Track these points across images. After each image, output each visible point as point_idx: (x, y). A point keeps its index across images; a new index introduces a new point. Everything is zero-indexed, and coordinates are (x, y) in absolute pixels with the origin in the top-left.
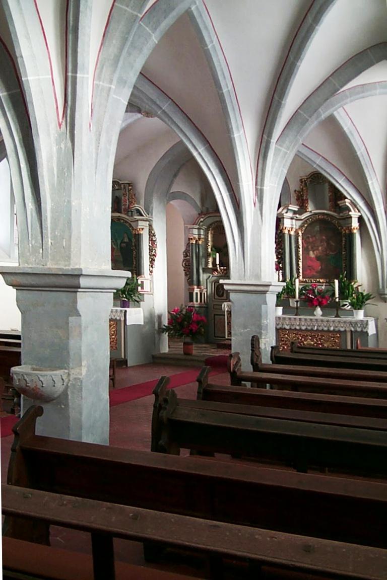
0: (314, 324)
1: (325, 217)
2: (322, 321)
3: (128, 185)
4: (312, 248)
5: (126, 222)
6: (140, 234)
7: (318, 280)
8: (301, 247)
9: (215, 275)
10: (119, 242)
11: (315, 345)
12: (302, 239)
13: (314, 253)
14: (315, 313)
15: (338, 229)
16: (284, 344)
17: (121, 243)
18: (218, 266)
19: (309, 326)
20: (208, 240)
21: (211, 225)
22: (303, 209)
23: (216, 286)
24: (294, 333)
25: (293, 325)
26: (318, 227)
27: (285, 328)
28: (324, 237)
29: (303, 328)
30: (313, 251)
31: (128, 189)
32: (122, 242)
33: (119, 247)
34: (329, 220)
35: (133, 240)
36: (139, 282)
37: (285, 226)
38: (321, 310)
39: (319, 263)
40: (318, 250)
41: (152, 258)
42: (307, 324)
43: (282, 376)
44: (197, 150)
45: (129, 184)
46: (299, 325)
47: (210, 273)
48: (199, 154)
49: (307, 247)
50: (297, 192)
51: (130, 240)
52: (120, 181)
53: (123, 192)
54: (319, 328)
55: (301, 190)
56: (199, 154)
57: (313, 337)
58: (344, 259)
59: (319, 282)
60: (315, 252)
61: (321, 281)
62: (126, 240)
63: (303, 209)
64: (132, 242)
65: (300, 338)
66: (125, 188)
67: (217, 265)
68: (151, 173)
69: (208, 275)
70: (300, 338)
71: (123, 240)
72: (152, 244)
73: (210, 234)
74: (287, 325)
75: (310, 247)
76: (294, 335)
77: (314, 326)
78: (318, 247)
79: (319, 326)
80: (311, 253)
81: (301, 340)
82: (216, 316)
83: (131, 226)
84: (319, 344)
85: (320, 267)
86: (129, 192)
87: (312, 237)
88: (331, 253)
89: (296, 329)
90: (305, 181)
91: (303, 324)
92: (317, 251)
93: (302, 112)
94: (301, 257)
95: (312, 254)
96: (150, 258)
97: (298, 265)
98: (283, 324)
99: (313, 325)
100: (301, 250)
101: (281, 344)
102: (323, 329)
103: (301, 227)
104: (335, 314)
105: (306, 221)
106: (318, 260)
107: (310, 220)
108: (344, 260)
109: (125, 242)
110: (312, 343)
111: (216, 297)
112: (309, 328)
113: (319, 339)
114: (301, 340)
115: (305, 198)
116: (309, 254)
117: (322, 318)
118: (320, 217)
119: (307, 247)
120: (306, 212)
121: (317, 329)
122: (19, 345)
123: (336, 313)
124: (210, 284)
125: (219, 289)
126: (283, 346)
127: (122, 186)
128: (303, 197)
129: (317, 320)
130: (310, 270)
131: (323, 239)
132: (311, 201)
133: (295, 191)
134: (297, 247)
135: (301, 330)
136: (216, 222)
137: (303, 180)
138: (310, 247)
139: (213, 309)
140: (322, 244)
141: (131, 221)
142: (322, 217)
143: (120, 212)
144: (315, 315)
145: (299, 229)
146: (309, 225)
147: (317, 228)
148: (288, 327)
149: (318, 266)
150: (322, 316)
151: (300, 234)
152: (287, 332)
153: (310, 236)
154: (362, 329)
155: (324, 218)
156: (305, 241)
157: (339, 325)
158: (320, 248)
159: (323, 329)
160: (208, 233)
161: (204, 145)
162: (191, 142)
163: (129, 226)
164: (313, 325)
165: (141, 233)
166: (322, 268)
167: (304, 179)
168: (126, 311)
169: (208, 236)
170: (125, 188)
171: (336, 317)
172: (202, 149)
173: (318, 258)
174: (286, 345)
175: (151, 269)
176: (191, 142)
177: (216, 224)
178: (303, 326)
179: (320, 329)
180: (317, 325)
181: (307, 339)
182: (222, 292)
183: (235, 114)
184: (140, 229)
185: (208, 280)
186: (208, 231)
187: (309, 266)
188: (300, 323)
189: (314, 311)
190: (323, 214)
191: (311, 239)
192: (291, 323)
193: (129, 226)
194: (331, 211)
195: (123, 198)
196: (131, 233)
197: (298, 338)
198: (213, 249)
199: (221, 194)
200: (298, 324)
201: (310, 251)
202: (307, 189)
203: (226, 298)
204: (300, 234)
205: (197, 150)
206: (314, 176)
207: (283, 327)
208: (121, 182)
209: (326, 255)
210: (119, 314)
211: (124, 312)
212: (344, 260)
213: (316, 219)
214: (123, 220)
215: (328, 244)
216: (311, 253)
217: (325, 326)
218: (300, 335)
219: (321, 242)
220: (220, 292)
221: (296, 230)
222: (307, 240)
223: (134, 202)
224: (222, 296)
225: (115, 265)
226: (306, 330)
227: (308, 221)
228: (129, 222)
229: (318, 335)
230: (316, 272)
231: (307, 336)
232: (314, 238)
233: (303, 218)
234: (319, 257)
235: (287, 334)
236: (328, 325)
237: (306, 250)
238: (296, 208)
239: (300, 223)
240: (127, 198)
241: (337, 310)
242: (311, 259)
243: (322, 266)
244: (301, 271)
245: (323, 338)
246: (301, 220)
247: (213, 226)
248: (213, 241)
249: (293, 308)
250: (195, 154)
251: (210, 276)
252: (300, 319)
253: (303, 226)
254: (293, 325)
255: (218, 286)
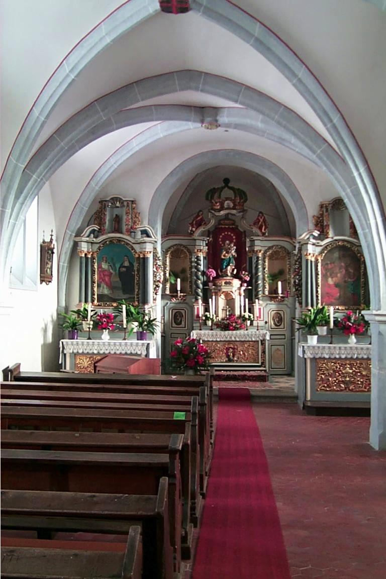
0: (354, 352)
1: (345, 243)
2: (357, 348)
3: (131, 202)
4: (331, 275)
5: (128, 244)
6: (147, 258)
7: (337, 307)
8: (320, 273)
9: (173, 302)
10: (118, 266)
11: (354, 373)
12: (322, 266)
13: (332, 280)
14: (349, 341)
15: (357, 256)
16: (322, 374)
17: (119, 268)
18: (179, 292)
19: (349, 354)
20: (166, 264)
21: (170, 248)
22: (323, 235)
23: (173, 314)
24: (332, 363)
25: (332, 354)
26: (337, 253)
27: (324, 357)
28: (343, 264)
29: (343, 357)
30: (332, 278)
31: (132, 206)
32: (122, 266)
33: (117, 271)
34: (349, 246)
35: (136, 265)
36: (147, 312)
37: (309, 252)
38: (355, 337)
39: (337, 290)
40: (337, 277)
41: (157, 284)
42: (358, 352)
43: (76, 403)
44: (358, 169)
45: (132, 201)
46: (339, 354)
47: (169, 300)
48: (360, 175)
49: (326, 273)
50: (315, 217)
51: (131, 264)
52: (124, 198)
53: (125, 209)
54: (358, 356)
55: (320, 216)
56: (360, 175)
57: (352, 366)
58: (363, 285)
59: (338, 309)
60: (334, 279)
61: (340, 308)
62: (126, 264)
63: (323, 235)
64: (133, 266)
65: (339, 367)
66: (128, 206)
67: (178, 291)
68: (157, 190)
69: (167, 301)
70: (339, 367)
71: (123, 263)
72: (156, 269)
73: (168, 258)
74: (327, 354)
75: (328, 274)
76: (333, 364)
77: (354, 355)
78: (337, 273)
79: (358, 354)
80: (330, 279)
81: (339, 368)
82: (273, 347)
83: (133, 249)
84: (358, 372)
85: (338, 294)
86: (132, 210)
87: (330, 263)
88: (349, 280)
89: (335, 358)
90: (326, 206)
91: (343, 352)
92: (336, 279)
93: (56, 136)
94: (320, 284)
95: (331, 281)
96: (154, 284)
97: (317, 292)
98: (322, 354)
99: (353, 353)
100: (320, 276)
101: (318, 374)
102: (363, 357)
103: (321, 253)
104: (88, 336)
105: (326, 247)
106: (336, 287)
107: (330, 246)
108: (363, 287)
109: (125, 267)
110: (351, 371)
111: (174, 325)
112: (349, 356)
113: (358, 367)
114: (339, 368)
115: (325, 224)
116: (327, 281)
117: (356, 346)
118: (340, 243)
119: (326, 273)
120: (327, 238)
121: (357, 357)
122: (3, 397)
123: (330, 340)
124: (168, 311)
125: (177, 316)
126: (321, 375)
127: (125, 203)
128: (323, 222)
129: (351, 348)
130: (328, 297)
131: (342, 266)
132: (332, 227)
133: (314, 217)
134: (317, 274)
135: (340, 358)
136: (175, 245)
137: (324, 205)
138: (328, 274)
139: (286, 340)
140: (341, 270)
141: (133, 243)
142: (342, 244)
143: (121, 233)
144: (349, 344)
145: (319, 255)
146: (329, 251)
147: (336, 255)
148: (327, 357)
149: (337, 293)
150: (356, 343)
151: (320, 261)
152: (326, 361)
153: (329, 262)
154: (368, 355)
155: (343, 245)
156: (324, 267)
157: (362, 353)
158: (339, 275)
159: (363, 357)
160: (166, 257)
161: (364, 165)
162: (354, 161)
163: (130, 249)
164: (353, 353)
165: (148, 256)
166: (340, 295)
167: (326, 204)
168: (148, 344)
169: (166, 261)
170: (128, 206)
171: (88, 339)
172: (362, 170)
173: (336, 285)
174: (323, 374)
175: (155, 296)
176: (354, 161)
177: (175, 247)
178: (343, 354)
179: (360, 357)
180: (356, 352)
181: (346, 368)
182: (180, 320)
183: (30, 133)
184: (257, 251)
185: (165, 307)
186: (167, 254)
187: (327, 293)
188: (339, 352)
189: (348, 339)
190: (344, 241)
191: (329, 265)
192: (358, 352)
193: (130, 249)
194: (352, 237)
195: (125, 217)
196: (133, 258)
197: (337, 367)
198: (171, 274)
199: (376, 219)
200: (338, 352)
201: (329, 277)
202: (328, 214)
203: (184, 326)
204: (320, 261)
205: (358, 169)
206: (336, 202)
207: (323, 356)
208: (124, 199)
209: (345, 282)
210: (129, 348)
211: (146, 345)
212: (363, 287)
213: (336, 245)
214: (124, 241)
215: (347, 270)
216: (330, 279)
217: (365, 354)
218: (339, 363)
219: (340, 269)
220: (178, 319)
221: (316, 256)
222: (326, 266)
223: (138, 222)
224: (180, 323)
225: (113, 292)
226: (346, 359)
227: (328, 247)
228: (131, 243)
229: (357, 363)
230: (335, 299)
231: (346, 365)
232: (333, 265)
233: (322, 244)
234: (338, 284)
235: (325, 364)
236: (368, 353)
237: (324, 277)
238: (316, 233)
239: (319, 249)
240: (130, 217)
241: (125, 333)
242: (329, 286)
243: (340, 293)
244: (320, 298)
245: (362, 366)
246: (321, 246)
247: (172, 249)
248: (171, 265)
249: (87, 331)
250: (356, 174)
251: (167, 303)
252: (340, 348)
253: (323, 253)
254: (332, 354)
255: (175, 313)
